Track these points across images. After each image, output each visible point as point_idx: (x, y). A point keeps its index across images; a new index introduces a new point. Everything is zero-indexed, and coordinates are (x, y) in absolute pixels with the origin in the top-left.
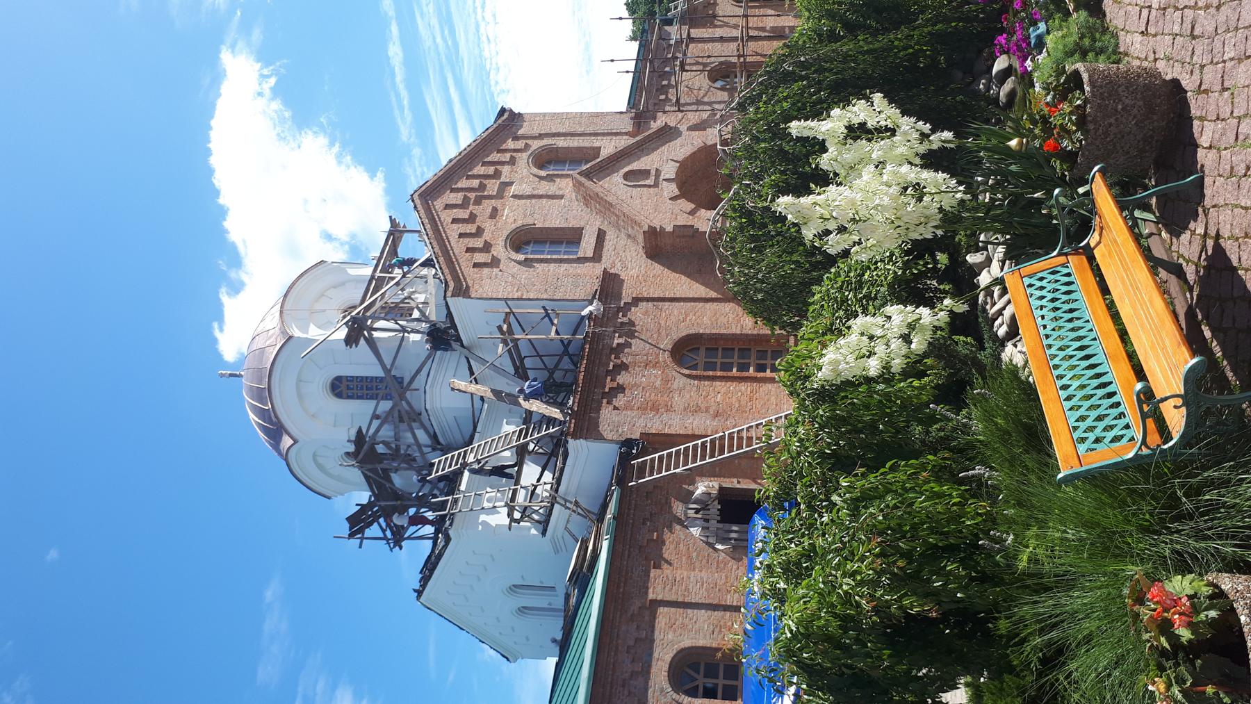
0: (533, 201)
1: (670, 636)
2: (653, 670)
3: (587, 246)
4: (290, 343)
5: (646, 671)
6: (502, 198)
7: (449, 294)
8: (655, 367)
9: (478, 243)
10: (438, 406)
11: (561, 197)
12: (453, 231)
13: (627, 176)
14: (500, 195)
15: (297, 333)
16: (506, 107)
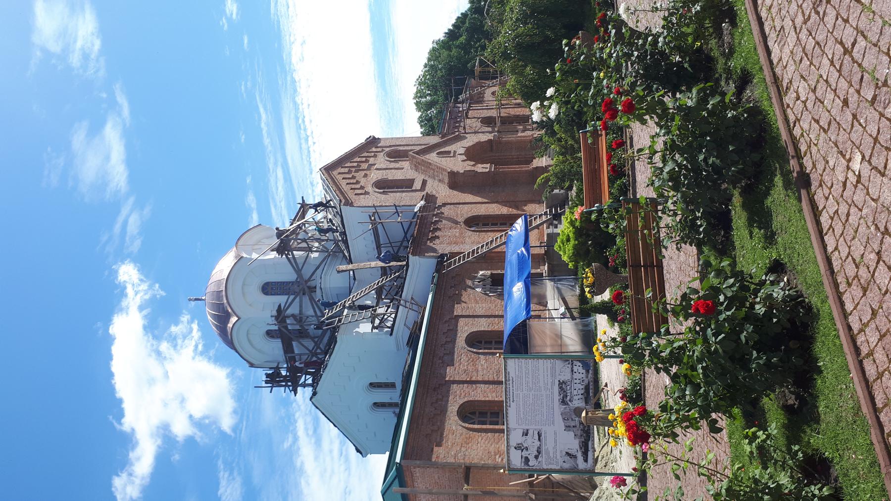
1: (466, 328)
2: (457, 341)
3: (417, 185)
4: (242, 259)
5: (453, 341)
7: (342, 204)
9: (358, 186)
10: (328, 286)
11: (403, 168)
14: (369, 168)
15: (245, 255)
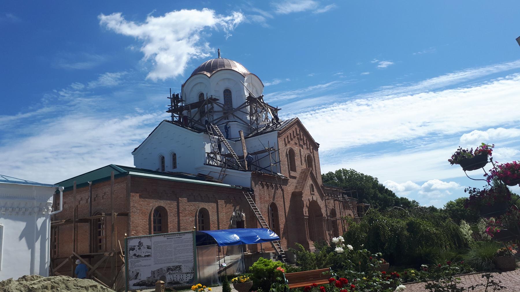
0: (300, 156)
2: (203, 203)
3: (293, 174)
4: (243, 77)
5: (203, 201)
6: (299, 146)
7: (279, 131)
8: (269, 197)
9: (289, 140)
11: (302, 165)
12: (290, 131)
13: (312, 184)
14: (300, 145)
16: (320, 146)
